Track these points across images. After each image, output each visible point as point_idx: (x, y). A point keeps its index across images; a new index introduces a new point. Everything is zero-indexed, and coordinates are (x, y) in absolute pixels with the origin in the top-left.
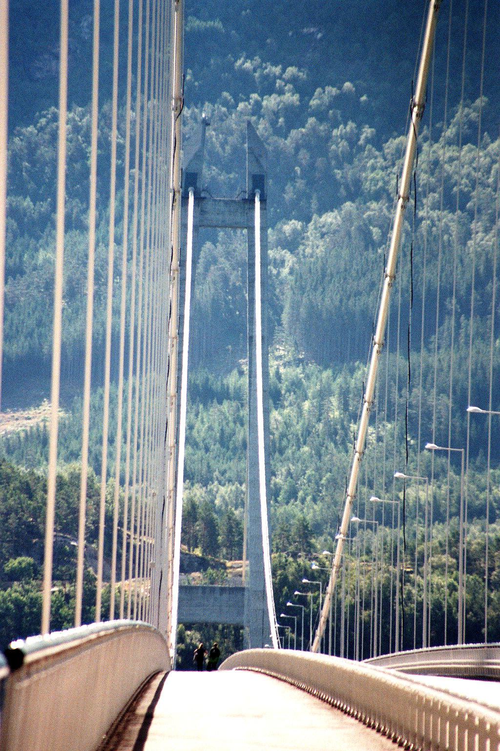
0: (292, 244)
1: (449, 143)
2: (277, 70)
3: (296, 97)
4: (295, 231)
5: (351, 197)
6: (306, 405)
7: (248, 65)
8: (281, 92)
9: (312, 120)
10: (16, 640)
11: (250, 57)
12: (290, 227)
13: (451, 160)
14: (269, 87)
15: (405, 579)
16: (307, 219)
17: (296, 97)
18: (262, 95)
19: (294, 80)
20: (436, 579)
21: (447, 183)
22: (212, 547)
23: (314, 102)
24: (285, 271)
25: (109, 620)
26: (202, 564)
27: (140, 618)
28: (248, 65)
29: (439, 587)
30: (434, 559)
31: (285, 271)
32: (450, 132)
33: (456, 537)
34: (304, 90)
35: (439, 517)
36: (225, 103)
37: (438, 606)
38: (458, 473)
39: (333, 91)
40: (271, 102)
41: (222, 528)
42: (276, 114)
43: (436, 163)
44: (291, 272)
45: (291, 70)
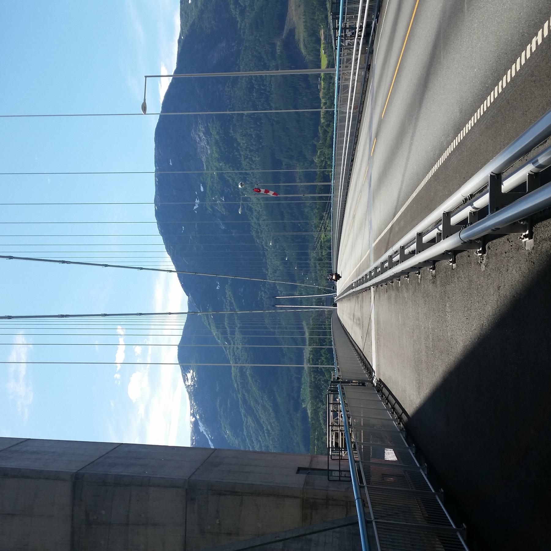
0: (281, 292)
1: (268, 272)
2: (259, 295)
3: (263, 292)
4: (280, 292)
5: (275, 284)
6: (302, 290)
7: (259, 298)
8: (262, 294)
9: (266, 290)
10: (116, 353)
11: (258, 298)
12: (279, 292)
13: (270, 272)
14: (262, 296)
15: (324, 277)
16: (278, 290)
17: (263, 292)
18: (262, 296)
19: (261, 293)
20: (324, 273)
21: (273, 272)
22: (321, 302)
23: (263, 290)
24: (285, 293)
25: (298, 467)
26: (323, 303)
27: (370, 8)
28: (259, 298)
29: (325, 272)
30: (322, 273)
31: (285, 293)
32: (267, 272)
33: (319, 270)
34: (262, 291)
35: (316, 272)
36: (263, 301)
37: (328, 272)
38: (310, 270)
39: (262, 288)
40: (263, 295)
41: (318, 300)
42: (265, 294)
43: (271, 274)
44: (285, 292)
45: (259, 293)
